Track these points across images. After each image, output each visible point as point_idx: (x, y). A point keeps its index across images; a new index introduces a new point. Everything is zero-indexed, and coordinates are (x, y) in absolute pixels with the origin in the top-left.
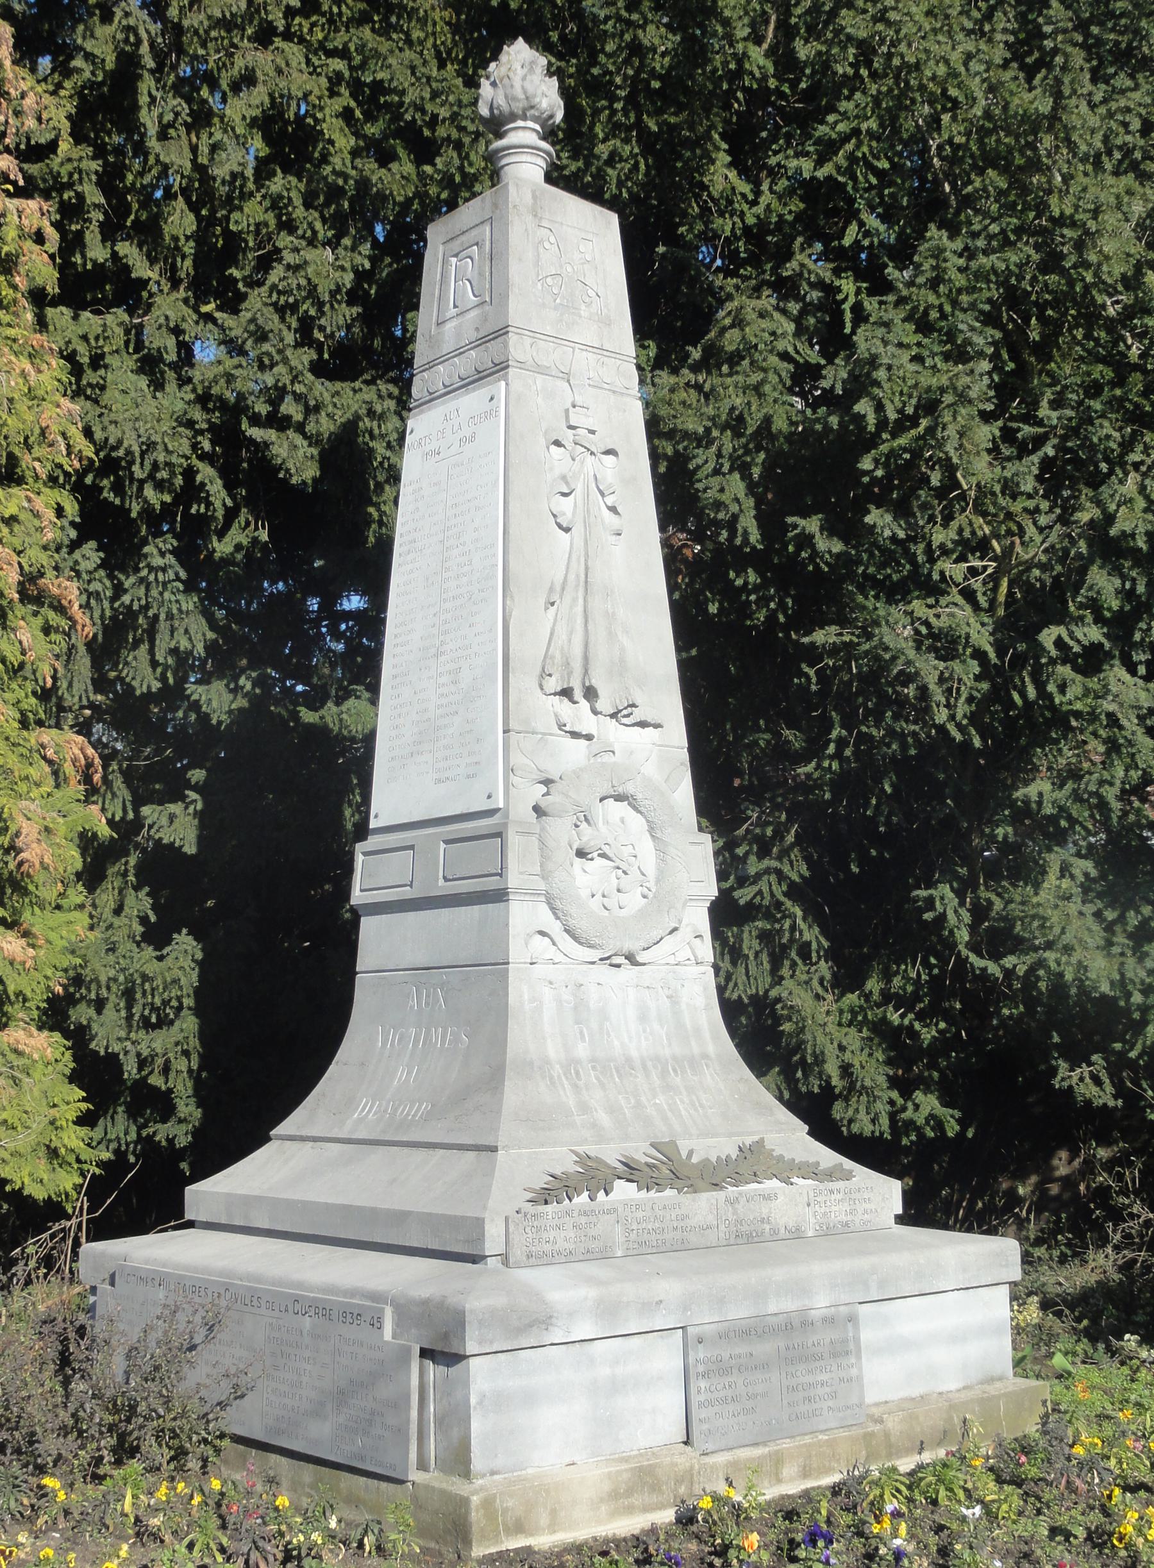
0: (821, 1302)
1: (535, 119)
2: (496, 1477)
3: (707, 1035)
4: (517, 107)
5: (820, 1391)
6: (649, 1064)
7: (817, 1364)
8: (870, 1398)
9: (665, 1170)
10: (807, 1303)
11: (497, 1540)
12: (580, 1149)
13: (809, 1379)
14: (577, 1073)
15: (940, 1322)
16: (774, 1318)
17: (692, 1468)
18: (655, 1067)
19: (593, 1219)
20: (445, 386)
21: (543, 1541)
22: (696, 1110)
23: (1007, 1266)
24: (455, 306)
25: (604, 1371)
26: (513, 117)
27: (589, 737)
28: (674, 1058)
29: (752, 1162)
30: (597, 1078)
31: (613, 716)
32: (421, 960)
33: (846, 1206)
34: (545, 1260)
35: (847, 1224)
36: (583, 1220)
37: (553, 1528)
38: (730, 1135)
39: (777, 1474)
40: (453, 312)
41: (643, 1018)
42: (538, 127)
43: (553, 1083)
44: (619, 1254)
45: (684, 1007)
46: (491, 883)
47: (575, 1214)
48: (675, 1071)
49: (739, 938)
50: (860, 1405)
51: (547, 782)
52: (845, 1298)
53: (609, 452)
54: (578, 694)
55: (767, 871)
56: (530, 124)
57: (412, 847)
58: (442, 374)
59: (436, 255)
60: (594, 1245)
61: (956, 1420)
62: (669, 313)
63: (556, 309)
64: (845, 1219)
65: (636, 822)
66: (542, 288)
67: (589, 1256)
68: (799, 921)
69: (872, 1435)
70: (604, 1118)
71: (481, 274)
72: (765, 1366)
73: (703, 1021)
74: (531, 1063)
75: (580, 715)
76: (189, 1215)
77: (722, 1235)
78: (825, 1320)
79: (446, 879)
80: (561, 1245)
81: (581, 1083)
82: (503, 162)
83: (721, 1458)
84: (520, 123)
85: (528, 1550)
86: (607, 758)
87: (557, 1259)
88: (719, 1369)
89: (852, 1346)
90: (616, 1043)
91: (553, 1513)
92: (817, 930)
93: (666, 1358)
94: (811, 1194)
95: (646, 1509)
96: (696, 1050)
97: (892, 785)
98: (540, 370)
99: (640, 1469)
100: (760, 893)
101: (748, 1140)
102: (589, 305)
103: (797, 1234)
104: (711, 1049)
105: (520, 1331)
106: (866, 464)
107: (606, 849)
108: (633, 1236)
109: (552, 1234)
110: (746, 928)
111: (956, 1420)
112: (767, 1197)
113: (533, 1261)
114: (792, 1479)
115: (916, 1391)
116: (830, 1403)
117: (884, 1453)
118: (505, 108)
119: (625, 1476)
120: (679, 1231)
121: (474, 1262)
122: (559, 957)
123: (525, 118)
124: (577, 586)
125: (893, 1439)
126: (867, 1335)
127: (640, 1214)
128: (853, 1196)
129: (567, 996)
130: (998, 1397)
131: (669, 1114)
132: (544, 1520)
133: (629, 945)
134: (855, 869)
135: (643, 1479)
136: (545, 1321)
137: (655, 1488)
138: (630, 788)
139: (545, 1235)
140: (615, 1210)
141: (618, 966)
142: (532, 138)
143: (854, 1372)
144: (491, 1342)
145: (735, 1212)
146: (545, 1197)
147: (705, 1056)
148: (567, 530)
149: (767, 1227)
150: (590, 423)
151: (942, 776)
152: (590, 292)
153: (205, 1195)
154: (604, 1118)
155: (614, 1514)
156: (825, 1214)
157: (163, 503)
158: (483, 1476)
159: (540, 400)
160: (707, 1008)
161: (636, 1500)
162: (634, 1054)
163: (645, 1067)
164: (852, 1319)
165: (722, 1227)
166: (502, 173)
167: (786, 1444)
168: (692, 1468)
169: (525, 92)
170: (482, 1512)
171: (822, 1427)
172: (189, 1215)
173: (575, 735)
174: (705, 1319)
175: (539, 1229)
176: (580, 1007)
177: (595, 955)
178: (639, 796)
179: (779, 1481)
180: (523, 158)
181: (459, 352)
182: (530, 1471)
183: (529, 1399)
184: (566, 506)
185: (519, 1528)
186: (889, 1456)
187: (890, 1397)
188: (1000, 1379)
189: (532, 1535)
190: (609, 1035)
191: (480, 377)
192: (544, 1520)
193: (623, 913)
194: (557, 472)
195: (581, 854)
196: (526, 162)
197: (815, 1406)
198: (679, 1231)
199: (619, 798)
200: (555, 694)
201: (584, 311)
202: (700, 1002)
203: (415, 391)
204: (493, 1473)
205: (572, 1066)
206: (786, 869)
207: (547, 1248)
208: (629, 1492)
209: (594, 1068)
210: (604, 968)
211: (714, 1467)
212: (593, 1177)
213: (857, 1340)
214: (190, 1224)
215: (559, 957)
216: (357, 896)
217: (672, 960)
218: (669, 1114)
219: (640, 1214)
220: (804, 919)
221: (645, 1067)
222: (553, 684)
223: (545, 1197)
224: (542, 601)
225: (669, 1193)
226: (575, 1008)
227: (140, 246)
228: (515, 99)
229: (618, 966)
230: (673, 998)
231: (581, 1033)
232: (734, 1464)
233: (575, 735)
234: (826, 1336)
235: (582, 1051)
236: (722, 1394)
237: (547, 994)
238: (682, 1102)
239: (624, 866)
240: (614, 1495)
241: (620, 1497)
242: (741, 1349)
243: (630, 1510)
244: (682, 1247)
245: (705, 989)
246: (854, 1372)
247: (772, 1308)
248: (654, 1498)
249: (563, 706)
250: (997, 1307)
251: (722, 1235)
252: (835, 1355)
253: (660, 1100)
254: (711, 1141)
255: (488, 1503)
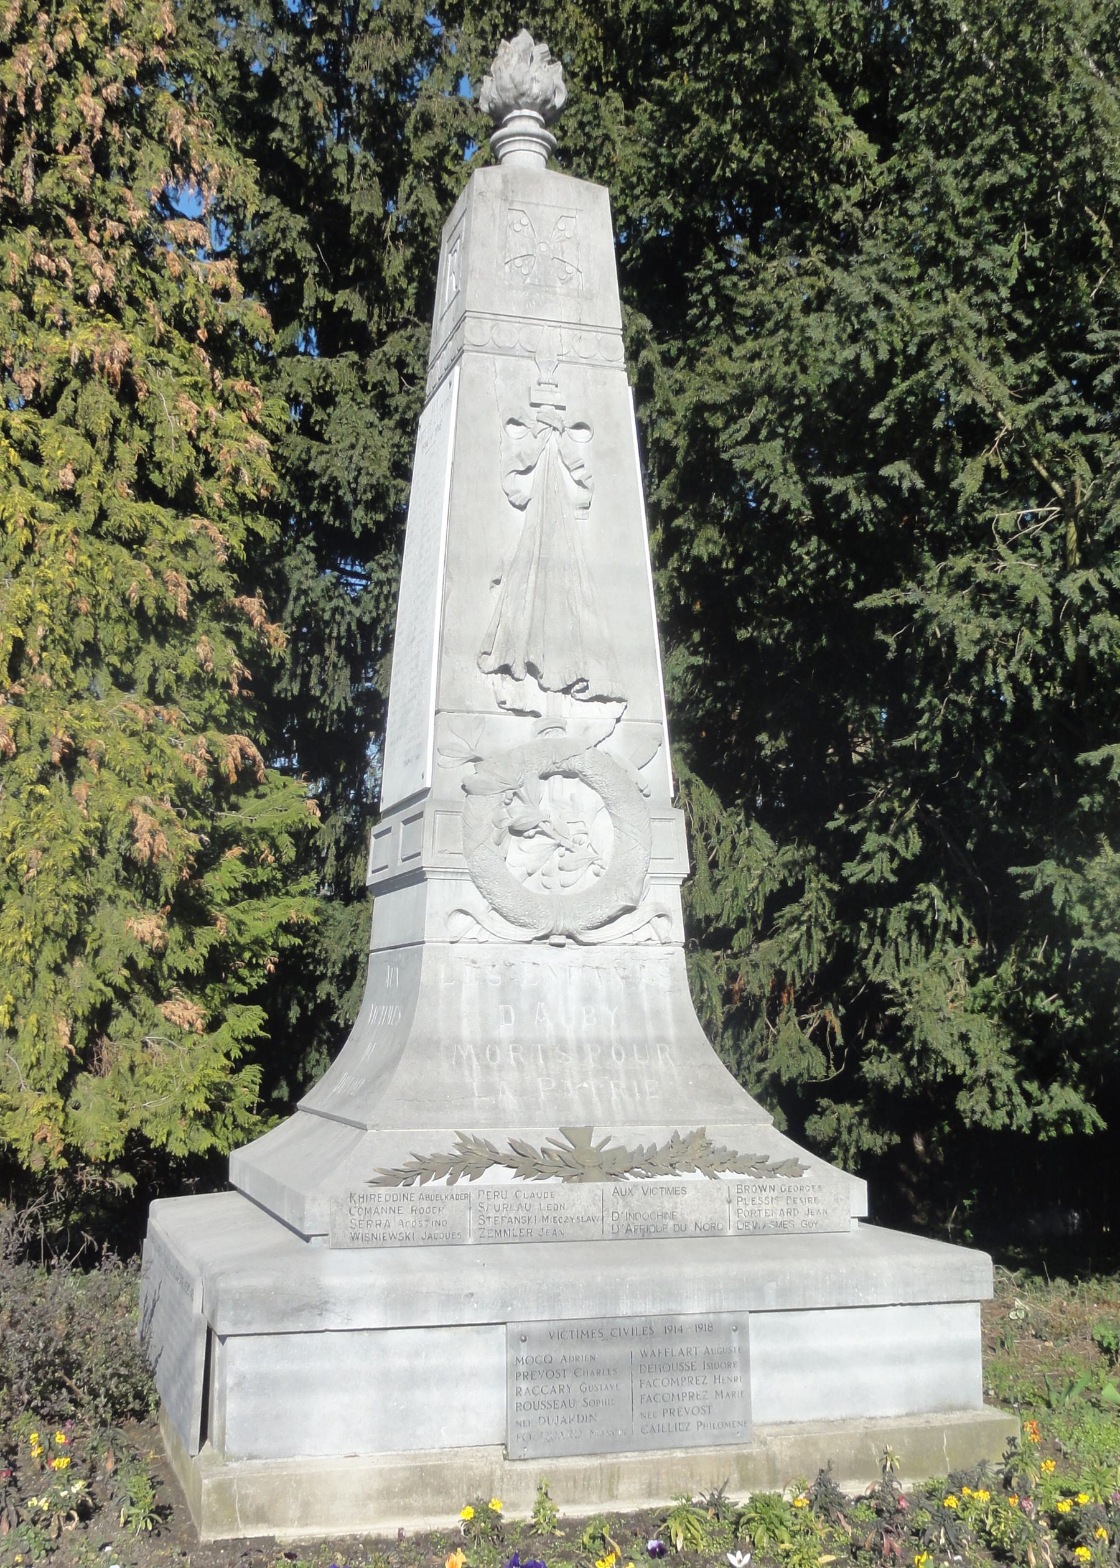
0: (694, 1308)
1: (531, 106)
2: (257, 1462)
3: (669, 1017)
4: (509, 97)
5: (688, 1404)
6: (587, 1047)
7: (685, 1374)
8: (757, 1416)
9: (577, 1160)
10: (674, 1307)
11: (232, 1526)
12: (467, 1132)
13: (674, 1389)
14: (493, 1055)
15: (884, 1337)
16: (627, 1322)
17: (492, 1473)
18: (594, 1050)
19: (439, 1204)
21: (288, 1534)
22: (632, 1095)
23: (972, 1282)
25: (401, 1362)
26: (508, 108)
27: (536, 714)
28: (621, 1041)
29: (693, 1152)
30: (516, 1059)
31: (566, 690)
33: (783, 1205)
34: (375, 1243)
35: (782, 1224)
36: (425, 1204)
37: (304, 1519)
38: (667, 1123)
39: (610, 1490)
41: (588, 998)
42: (535, 114)
43: (459, 1063)
44: (470, 1241)
45: (642, 987)
47: (415, 1197)
48: (618, 1054)
49: (885, 918)
50: (744, 1424)
51: (476, 760)
52: (728, 1305)
53: (579, 426)
54: (519, 670)
55: (882, 848)
56: (526, 112)
60: (437, 1231)
61: (874, 1451)
62: (660, 282)
63: (525, 288)
64: (780, 1219)
65: (589, 798)
66: (533, 268)
67: (429, 1241)
68: (938, 903)
69: (748, 1458)
70: (509, 1100)
72: (610, 1371)
73: (667, 1003)
74: (437, 1043)
75: (528, 693)
77: (607, 1228)
78: (699, 1327)
80: (395, 1228)
81: (494, 1064)
83: (533, 1466)
84: (516, 113)
85: (270, 1541)
86: (553, 735)
87: (389, 1243)
88: (549, 1370)
89: (736, 1358)
90: (549, 1024)
91: (306, 1505)
92: (959, 910)
93: (487, 1354)
94: (734, 1191)
95: (428, 1512)
96: (651, 1032)
97: (996, 756)
98: (503, 351)
99: (422, 1469)
100: (872, 871)
101: (684, 1132)
102: (565, 282)
103: (712, 1232)
104: (671, 1032)
105: (285, 1315)
106: (875, 413)
107: (544, 827)
108: (490, 1224)
109: (384, 1217)
110: (895, 910)
111: (874, 1451)
112: (673, 1191)
113: (357, 1243)
114: (631, 1497)
115: (837, 1414)
116: (701, 1418)
117: (765, 1478)
119: (401, 1475)
120: (550, 1223)
122: (492, 938)
123: (520, 108)
124: (530, 562)
125: (779, 1465)
126: (755, 1348)
127: (499, 1201)
128: (793, 1195)
129: (492, 975)
130: (940, 1430)
131: (595, 1099)
132: (293, 1511)
133: (572, 926)
134: (969, 846)
135: (426, 1481)
136: (321, 1306)
137: (442, 1489)
138: (575, 764)
139: (375, 1218)
140: (467, 1196)
141: (562, 946)
142: (534, 128)
143: (738, 1386)
144: (249, 1323)
145: (627, 1204)
146: (391, 1178)
147: (662, 1039)
148: (522, 508)
149: (671, 1223)
150: (559, 399)
151: (1032, 743)
152: (569, 269)
154: (509, 1100)
155: (385, 1513)
156: (752, 1212)
157: (376, 523)
158: (238, 1459)
159: (498, 381)
160: (673, 990)
161: (415, 1501)
162: (570, 1036)
163: (580, 1049)
164: (741, 1329)
165: (609, 1220)
167: (632, 1457)
168: (492, 1473)
169: (512, 79)
170: (213, 1497)
171: (686, 1443)
173: (519, 712)
174: (533, 1315)
175: (368, 1211)
176: (508, 988)
177: (528, 934)
178: (589, 772)
179: (612, 1496)
180: (516, 146)
182: (298, 1459)
183: (302, 1384)
184: (525, 485)
185: (261, 1516)
186: (773, 1483)
187: (796, 1417)
188: (964, 1408)
189: (276, 1525)
190: (541, 1015)
192: (293, 1511)
193: (566, 891)
194: (515, 450)
195: (516, 832)
196: (525, 151)
197: (679, 1420)
198: (550, 1223)
199: (569, 774)
200: (496, 672)
201: (560, 289)
202: (665, 983)
204: (251, 1457)
205: (487, 1048)
206: (899, 846)
207: (379, 1231)
208: (407, 1492)
209: (515, 1049)
210: (542, 948)
211: (522, 1476)
212: (471, 1159)
213: (744, 1353)
215: (485, 936)
217: (629, 939)
218: (595, 1099)
219: (499, 1201)
220: (946, 898)
221: (580, 1049)
222: (492, 662)
223: (391, 1178)
224: (488, 581)
225: (552, 1180)
226: (503, 988)
227: (361, 294)
229: (562, 946)
230: (629, 981)
231: (507, 1014)
232: (552, 1474)
233: (519, 712)
234: (700, 1345)
235: (504, 1032)
236: (550, 1397)
237: (469, 974)
238: (617, 1086)
239: (568, 843)
240: (387, 1493)
241: (395, 1493)
242: (582, 1351)
243: (406, 1511)
244: (555, 1238)
245: (672, 970)
246: (738, 1386)
247: (625, 1309)
248: (440, 1501)
249: (505, 687)
250: (967, 1326)
251: (607, 1228)
252: (711, 1366)
253: (591, 1085)
254: (640, 1129)
255: (222, 1489)
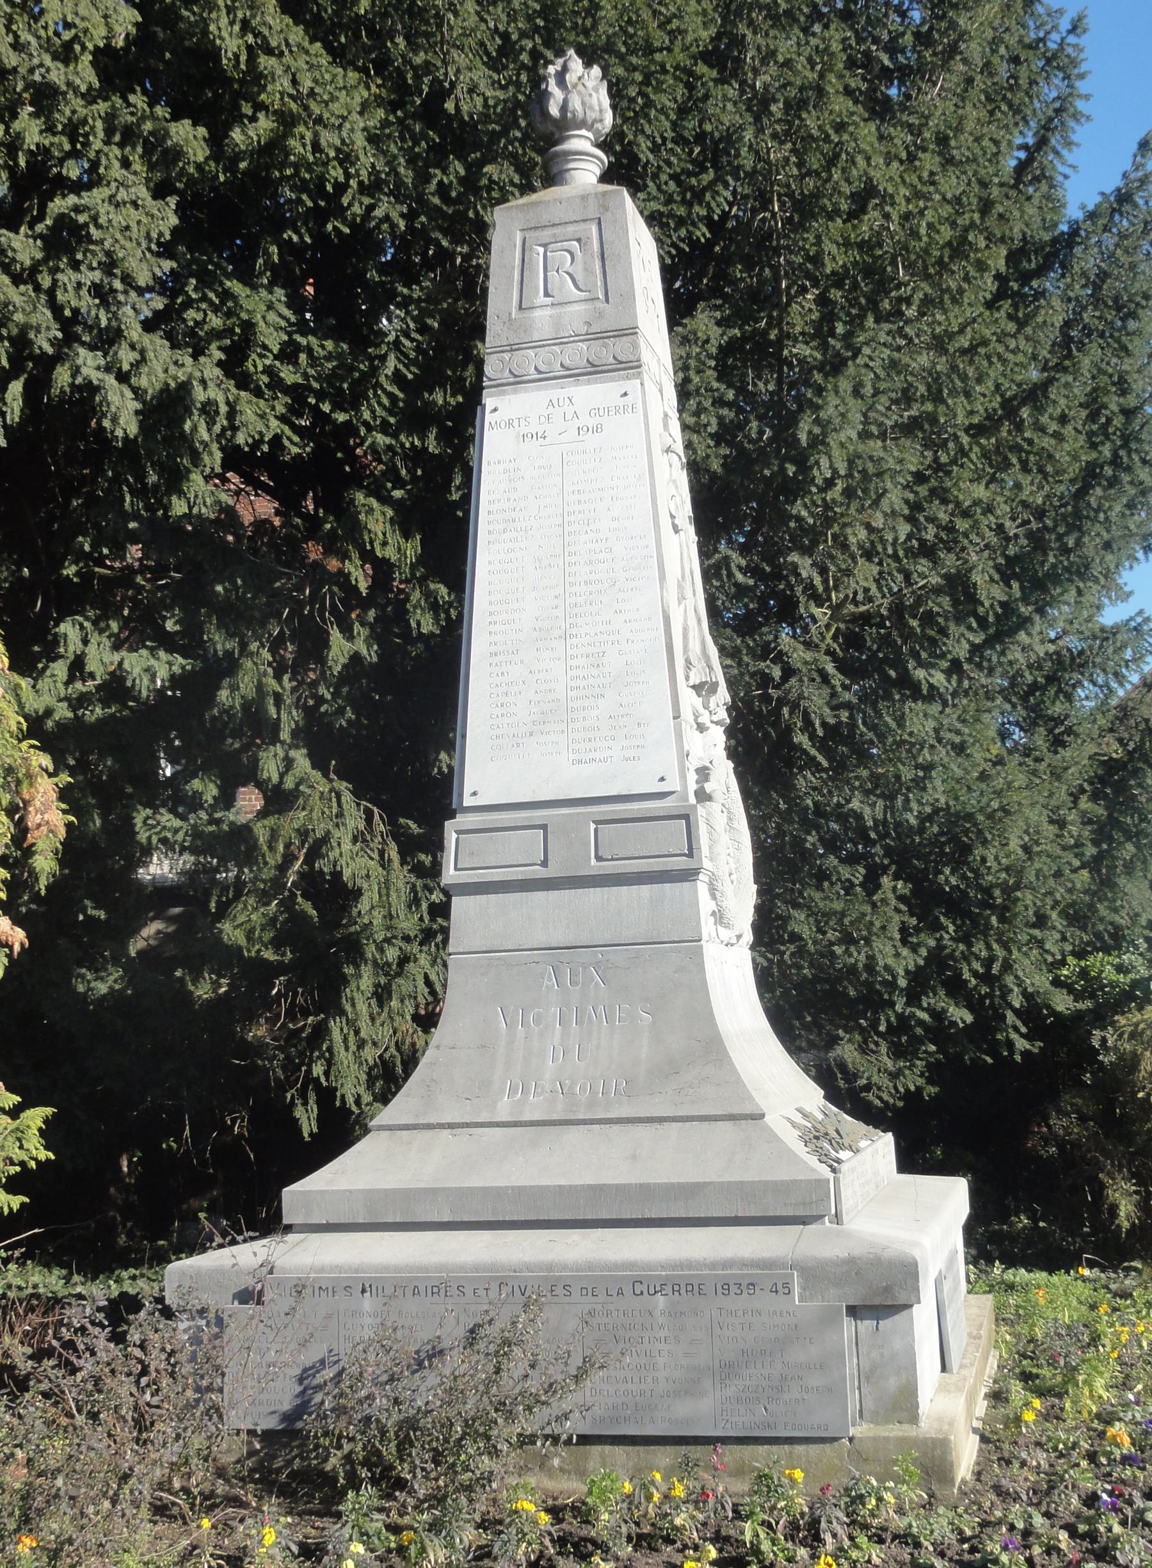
20: (539, 372)
24: (547, 294)
32: (559, 937)
40: (541, 299)
46: (680, 863)
57: (544, 827)
58: (529, 361)
59: (511, 239)
71: (588, 270)
76: (285, 1221)
79: (599, 858)
82: (571, 165)
84: (584, 132)
118: (580, 114)
121: (804, 1223)
153: (300, 1195)
166: (567, 175)
172: (285, 1221)
181: (560, 341)
191: (594, 370)
196: (586, 171)
203: (488, 370)
214: (288, 1229)
216: (450, 875)
228: (591, 108)
